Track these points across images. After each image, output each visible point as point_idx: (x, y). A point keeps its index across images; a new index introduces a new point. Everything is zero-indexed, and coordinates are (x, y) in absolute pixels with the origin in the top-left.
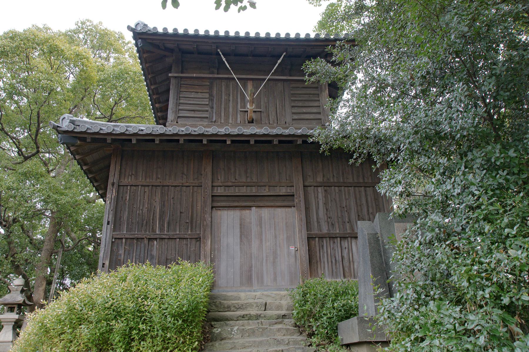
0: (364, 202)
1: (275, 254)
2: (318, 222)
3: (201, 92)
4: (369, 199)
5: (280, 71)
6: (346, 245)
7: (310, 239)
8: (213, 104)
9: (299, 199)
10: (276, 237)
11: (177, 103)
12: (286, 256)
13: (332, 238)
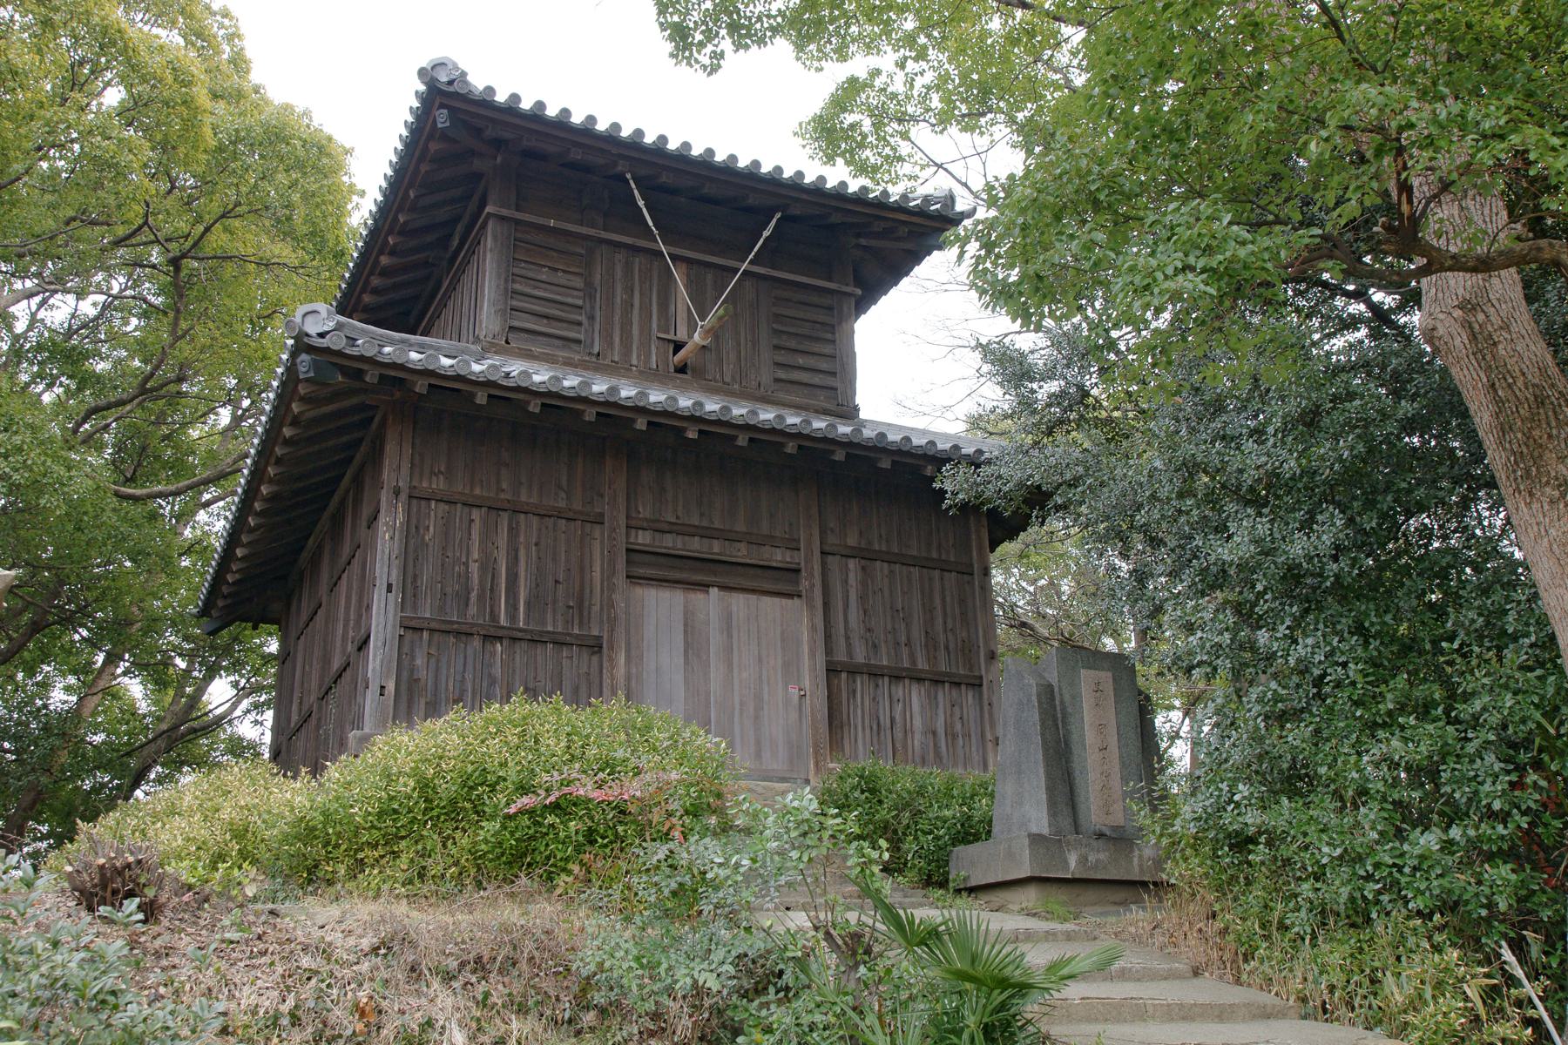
0: (938, 601)
1: (758, 698)
2: (847, 638)
3: (564, 271)
4: (948, 599)
5: (770, 254)
6: (900, 692)
7: (832, 670)
8: (593, 308)
9: (810, 581)
10: (760, 660)
11: (506, 289)
12: (780, 705)
13: (875, 674)
